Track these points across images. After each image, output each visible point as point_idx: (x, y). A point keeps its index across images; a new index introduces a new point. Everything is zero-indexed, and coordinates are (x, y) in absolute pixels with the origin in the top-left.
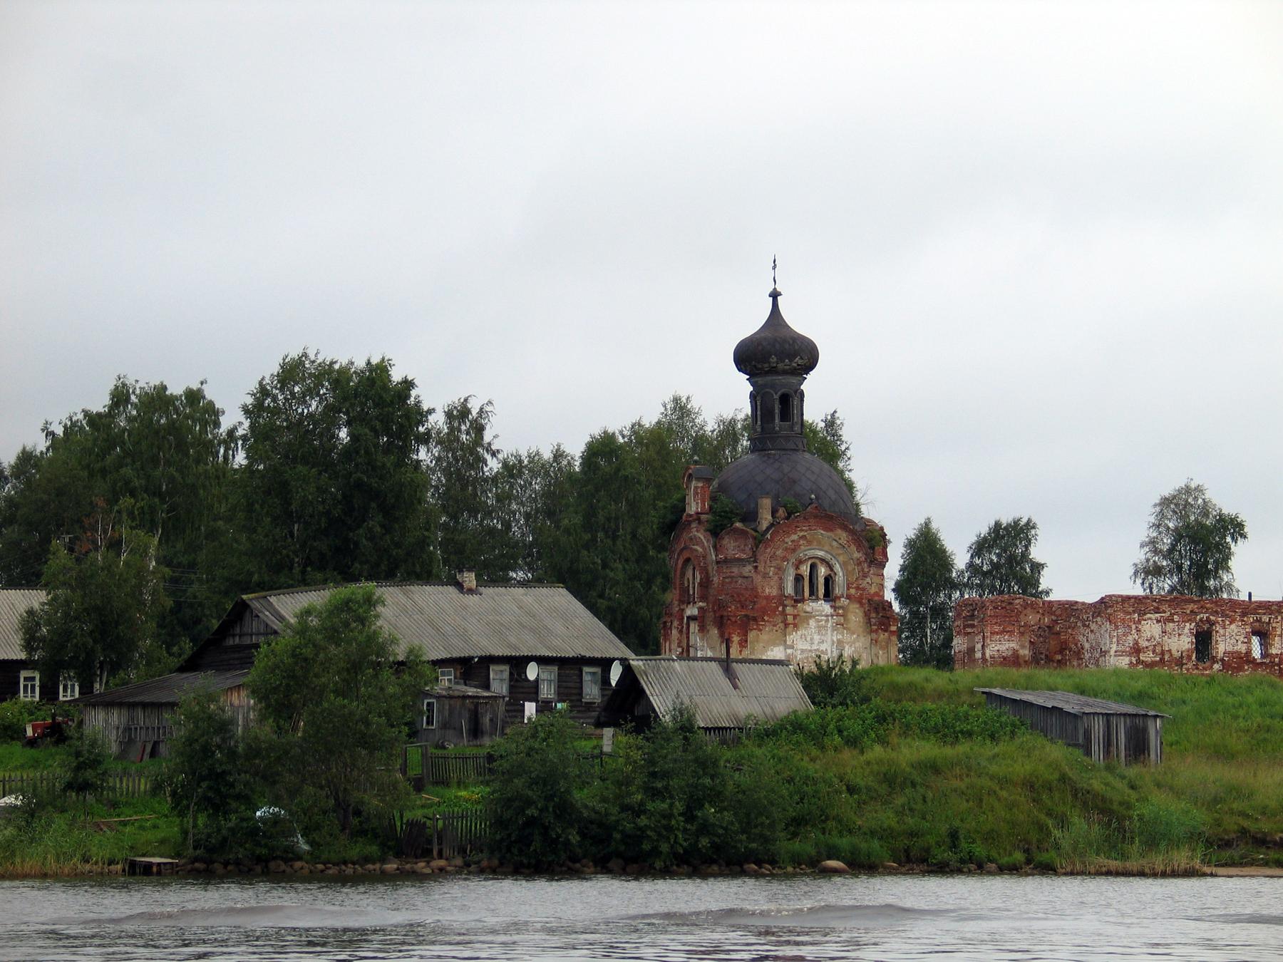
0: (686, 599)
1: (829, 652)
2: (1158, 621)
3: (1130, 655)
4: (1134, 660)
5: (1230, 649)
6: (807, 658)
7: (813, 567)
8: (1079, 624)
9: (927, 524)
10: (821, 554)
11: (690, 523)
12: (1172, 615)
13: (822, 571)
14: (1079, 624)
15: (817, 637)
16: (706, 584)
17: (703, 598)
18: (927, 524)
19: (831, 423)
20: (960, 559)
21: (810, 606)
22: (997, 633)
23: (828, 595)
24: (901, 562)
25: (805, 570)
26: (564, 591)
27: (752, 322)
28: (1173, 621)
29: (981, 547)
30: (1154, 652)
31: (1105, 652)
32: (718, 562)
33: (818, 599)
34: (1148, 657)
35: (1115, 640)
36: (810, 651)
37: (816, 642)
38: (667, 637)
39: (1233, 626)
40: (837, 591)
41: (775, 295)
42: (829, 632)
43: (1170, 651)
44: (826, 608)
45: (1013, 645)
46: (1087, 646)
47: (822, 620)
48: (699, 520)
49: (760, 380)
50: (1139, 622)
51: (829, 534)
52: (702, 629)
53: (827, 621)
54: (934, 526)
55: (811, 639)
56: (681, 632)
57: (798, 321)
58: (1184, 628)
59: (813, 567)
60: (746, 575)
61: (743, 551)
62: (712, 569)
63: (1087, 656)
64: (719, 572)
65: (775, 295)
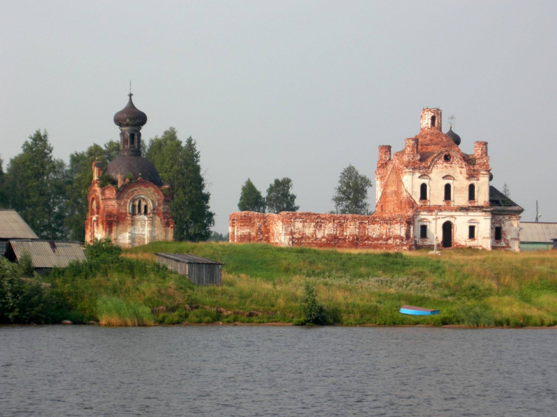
0: (92, 214)
2: (301, 222)
3: (289, 235)
4: (291, 237)
5: (329, 233)
7: (140, 202)
8: (274, 223)
9: (249, 179)
10: (143, 196)
11: (94, 184)
12: (306, 220)
13: (143, 204)
14: (274, 223)
15: (141, 229)
16: (98, 208)
17: (98, 213)
18: (249, 179)
19: (189, 141)
20: (264, 194)
21: (138, 217)
22: (242, 226)
23: (146, 213)
24: (241, 195)
25: (137, 203)
26: (15, 212)
27: (123, 105)
28: (306, 222)
29: (271, 190)
30: (299, 234)
31: (281, 234)
32: (102, 199)
33: (141, 214)
34: (297, 236)
35: (284, 229)
37: (140, 231)
38: (87, 228)
39: (330, 224)
40: (149, 211)
41: (131, 95)
42: (146, 226)
43: (305, 233)
45: (248, 231)
46: (275, 231)
48: (97, 183)
49: (123, 128)
50: (294, 222)
51: (146, 189)
52: (97, 224)
53: (145, 223)
54: (251, 180)
56: (91, 226)
57: (140, 106)
58: (311, 224)
59: (140, 202)
60: (113, 204)
61: (112, 195)
62: (101, 202)
63: (275, 235)
64: (103, 203)
65: (131, 95)
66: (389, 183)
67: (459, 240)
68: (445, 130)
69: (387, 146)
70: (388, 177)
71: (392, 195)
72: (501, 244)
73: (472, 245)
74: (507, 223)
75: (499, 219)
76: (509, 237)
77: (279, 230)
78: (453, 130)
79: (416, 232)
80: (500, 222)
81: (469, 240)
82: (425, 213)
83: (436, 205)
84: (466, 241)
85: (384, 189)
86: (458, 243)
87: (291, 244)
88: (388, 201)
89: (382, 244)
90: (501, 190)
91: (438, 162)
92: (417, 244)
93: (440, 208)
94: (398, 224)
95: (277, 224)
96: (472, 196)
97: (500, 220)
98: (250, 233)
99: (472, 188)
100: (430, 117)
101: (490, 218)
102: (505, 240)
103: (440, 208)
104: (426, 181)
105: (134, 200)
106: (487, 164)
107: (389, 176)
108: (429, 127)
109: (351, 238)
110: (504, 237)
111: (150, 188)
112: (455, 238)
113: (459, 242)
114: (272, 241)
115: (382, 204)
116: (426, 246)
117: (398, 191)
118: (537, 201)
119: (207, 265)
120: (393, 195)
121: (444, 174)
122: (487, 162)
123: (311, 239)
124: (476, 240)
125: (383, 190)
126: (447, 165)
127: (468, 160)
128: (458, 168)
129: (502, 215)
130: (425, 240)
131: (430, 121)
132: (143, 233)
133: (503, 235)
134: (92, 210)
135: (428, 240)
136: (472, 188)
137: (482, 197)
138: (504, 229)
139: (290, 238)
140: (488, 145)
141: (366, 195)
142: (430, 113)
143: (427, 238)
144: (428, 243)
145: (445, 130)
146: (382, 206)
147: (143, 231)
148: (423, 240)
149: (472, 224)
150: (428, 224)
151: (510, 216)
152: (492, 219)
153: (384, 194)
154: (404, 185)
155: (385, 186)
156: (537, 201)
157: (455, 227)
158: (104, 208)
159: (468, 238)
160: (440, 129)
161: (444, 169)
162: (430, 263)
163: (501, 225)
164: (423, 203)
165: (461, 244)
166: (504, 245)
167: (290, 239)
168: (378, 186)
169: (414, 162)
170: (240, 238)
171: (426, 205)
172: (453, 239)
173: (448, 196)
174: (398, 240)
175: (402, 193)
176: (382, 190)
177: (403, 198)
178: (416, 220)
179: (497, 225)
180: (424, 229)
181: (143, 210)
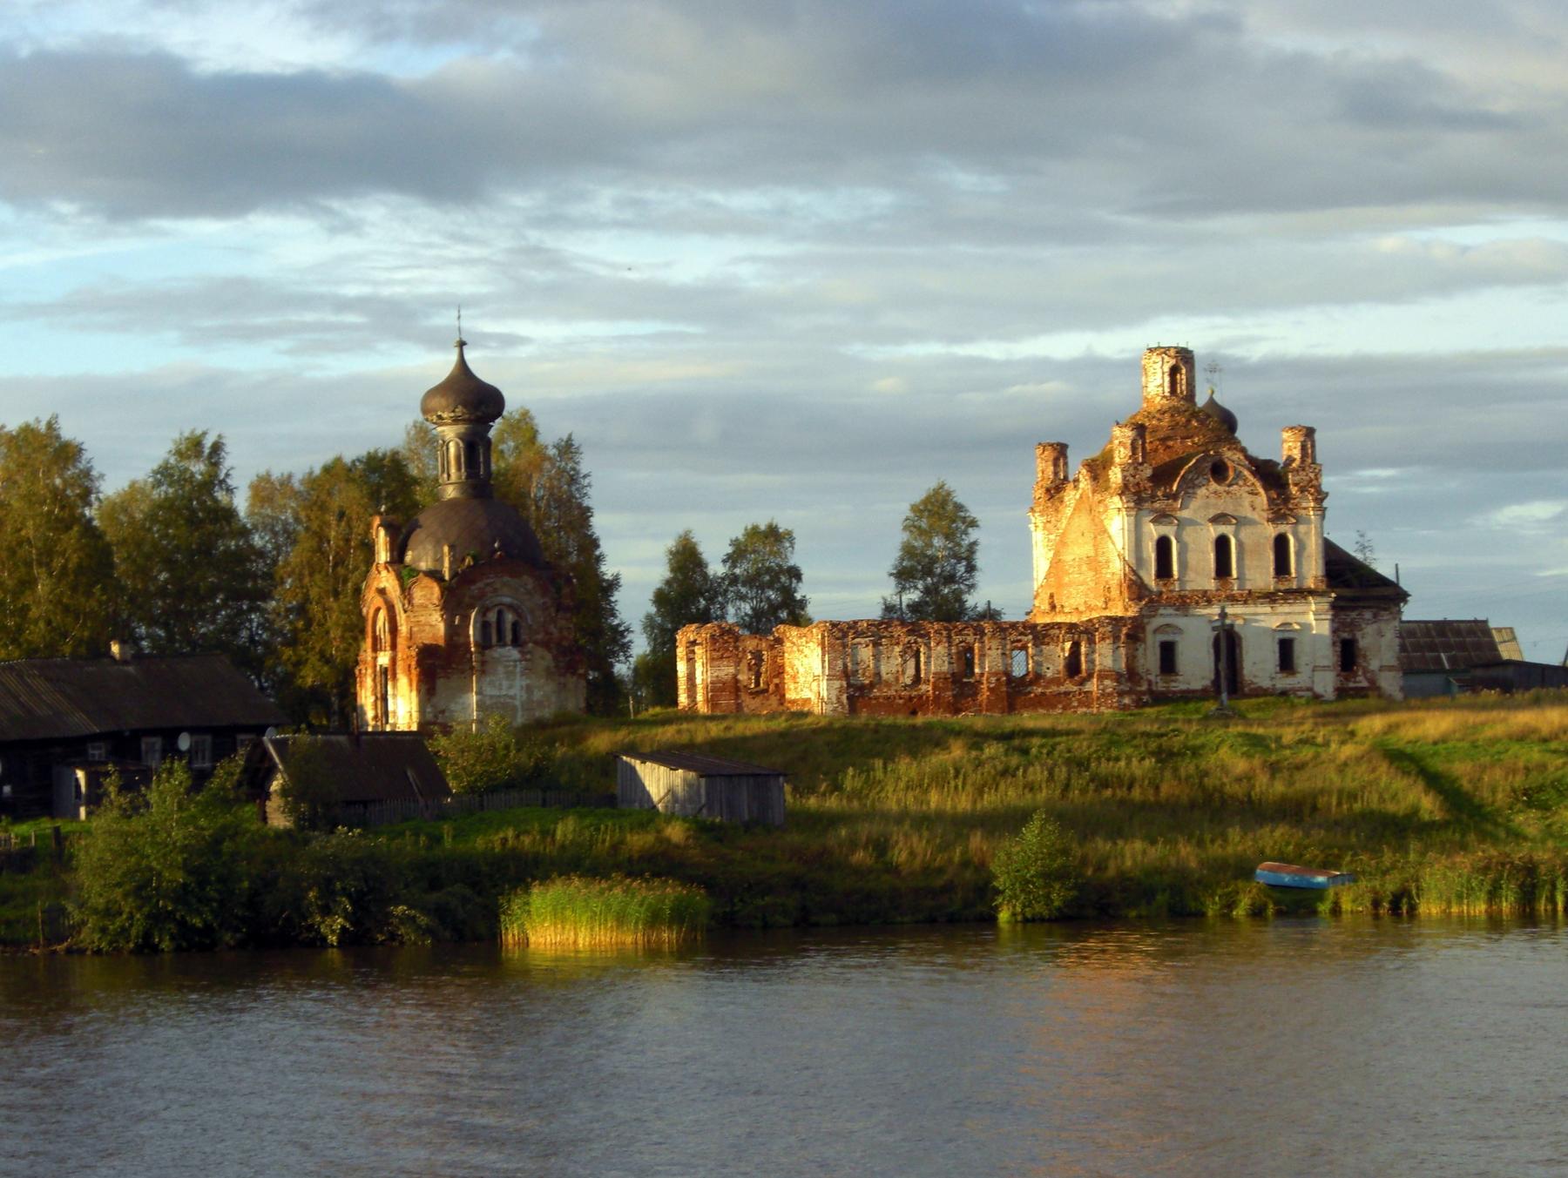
1: (518, 697)
4: (845, 684)
6: (496, 703)
13: (510, 617)
15: (505, 683)
21: (498, 652)
23: (516, 642)
25: (492, 617)
33: (505, 645)
35: (826, 664)
36: (499, 696)
37: (504, 687)
42: (518, 675)
44: (514, 653)
46: (801, 670)
47: (509, 666)
53: (515, 666)
55: (500, 685)
58: (892, 651)
59: (500, 613)
66: (1072, 536)
67: (1255, 676)
68: (1201, 400)
69: (1058, 444)
70: (1069, 524)
71: (1079, 566)
72: (1355, 682)
73: (1288, 686)
74: (1370, 629)
75: (1349, 620)
76: (1374, 665)
77: (811, 668)
78: (1217, 398)
79: (1150, 659)
80: (1353, 626)
81: (1279, 675)
82: (1170, 611)
83: (1197, 591)
84: (1272, 679)
85: (1057, 554)
86: (1252, 683)
87: (845, 701)
88: (1069, 585)
89: (1069, 693)
90: (1350, 548)
91: (1196, 482)
92: (1154, 688)
93: (1207, 598)
94: (1108, 641)
95: (806, 651)
96: (1282, 567)
97: (1353, 619)
98: (735, 677)
99: (1281, 543)
100: (1167, 368)
101: (1329, 617)
102: (1365, 671)
103: (1207, 598)
104: (1169, 531)
105: (484, 612)
106: (1314, 482)
107: (1071, 518)
108: (1167, 394)
109: (993, 679)
110: (1364, 664)
111: (525, 577)
112: (1245, 672)
113: (1255, 680)
114: (790, 695)
115: (1053, 590)
116: (1174, 692)
117: (1097, 555)
118: (1397, 565)
119: (751, 780)
120: (1084, 568)
121: (1212, 513)
122: (1317, 479)
123: (893, 688)
124: (1298, 675)
125: (1055, 554)
126: (1219, 488)
127: (1270, 475)
128: (1245, 495)
129: (1354, 609)
130: (1173, 678)
131: (1167, 379)
132: (512, 692)
133: (1360, 661)
134: (376, 639)
135: (1180, 678)
136: (1281, 543)
137: (1310, 570)
138: (1363, 643)
139: (842, 687)
140: (1317, 436)
141: (255, 478)
142: (1166, 358)
143: (1177, 674)
144: (1180, 685)
145: (1201, 400)
146: (1052, 596)
147: (510, 687)
148: (1168, 678)
149: (1286, 635)
150: (1177, 638)
151: (1374, 610)
152: (1333, 621)
153: (1056, 564)
154: (1113, 543)
155: (1060, 546)
156: (1397, 565)
157: (1244, 644)
158: (411, 632)
159: (1278, 668)
160: (1190, 397)
161: (1213, 500)
162: (1422, 763)
163: (1354, 635)
164: (1165, 585)
165: (1260, 684)
166: (1365, 684)
167: (841, 690)
168: (1040, 544)
169: (1138, 484)
170: (712, 691)
171: (1171, 591)
172: (1242, 675)
173: (1223, 569)
174: (1107, 682)
175: (1108, 562)
176: (1051, 554)
177: (1113, 574)
178: (1150, 629)
179: (1345, 635)
180: (1168, 652)
181: (509, 637)
